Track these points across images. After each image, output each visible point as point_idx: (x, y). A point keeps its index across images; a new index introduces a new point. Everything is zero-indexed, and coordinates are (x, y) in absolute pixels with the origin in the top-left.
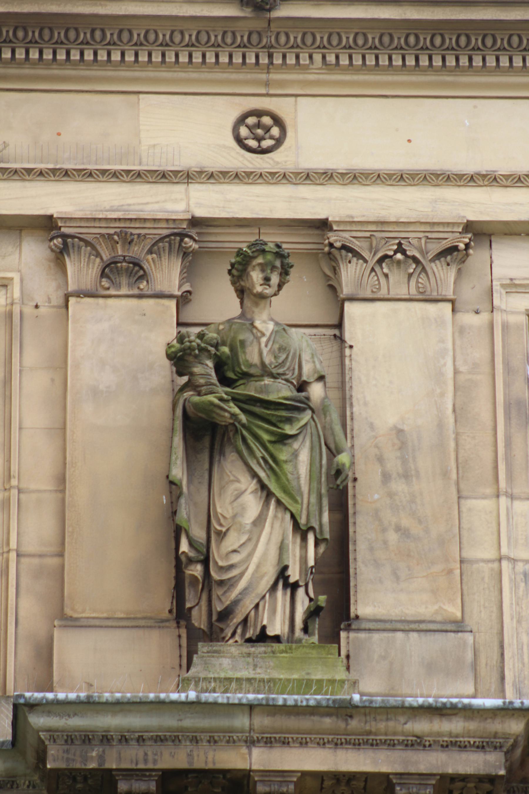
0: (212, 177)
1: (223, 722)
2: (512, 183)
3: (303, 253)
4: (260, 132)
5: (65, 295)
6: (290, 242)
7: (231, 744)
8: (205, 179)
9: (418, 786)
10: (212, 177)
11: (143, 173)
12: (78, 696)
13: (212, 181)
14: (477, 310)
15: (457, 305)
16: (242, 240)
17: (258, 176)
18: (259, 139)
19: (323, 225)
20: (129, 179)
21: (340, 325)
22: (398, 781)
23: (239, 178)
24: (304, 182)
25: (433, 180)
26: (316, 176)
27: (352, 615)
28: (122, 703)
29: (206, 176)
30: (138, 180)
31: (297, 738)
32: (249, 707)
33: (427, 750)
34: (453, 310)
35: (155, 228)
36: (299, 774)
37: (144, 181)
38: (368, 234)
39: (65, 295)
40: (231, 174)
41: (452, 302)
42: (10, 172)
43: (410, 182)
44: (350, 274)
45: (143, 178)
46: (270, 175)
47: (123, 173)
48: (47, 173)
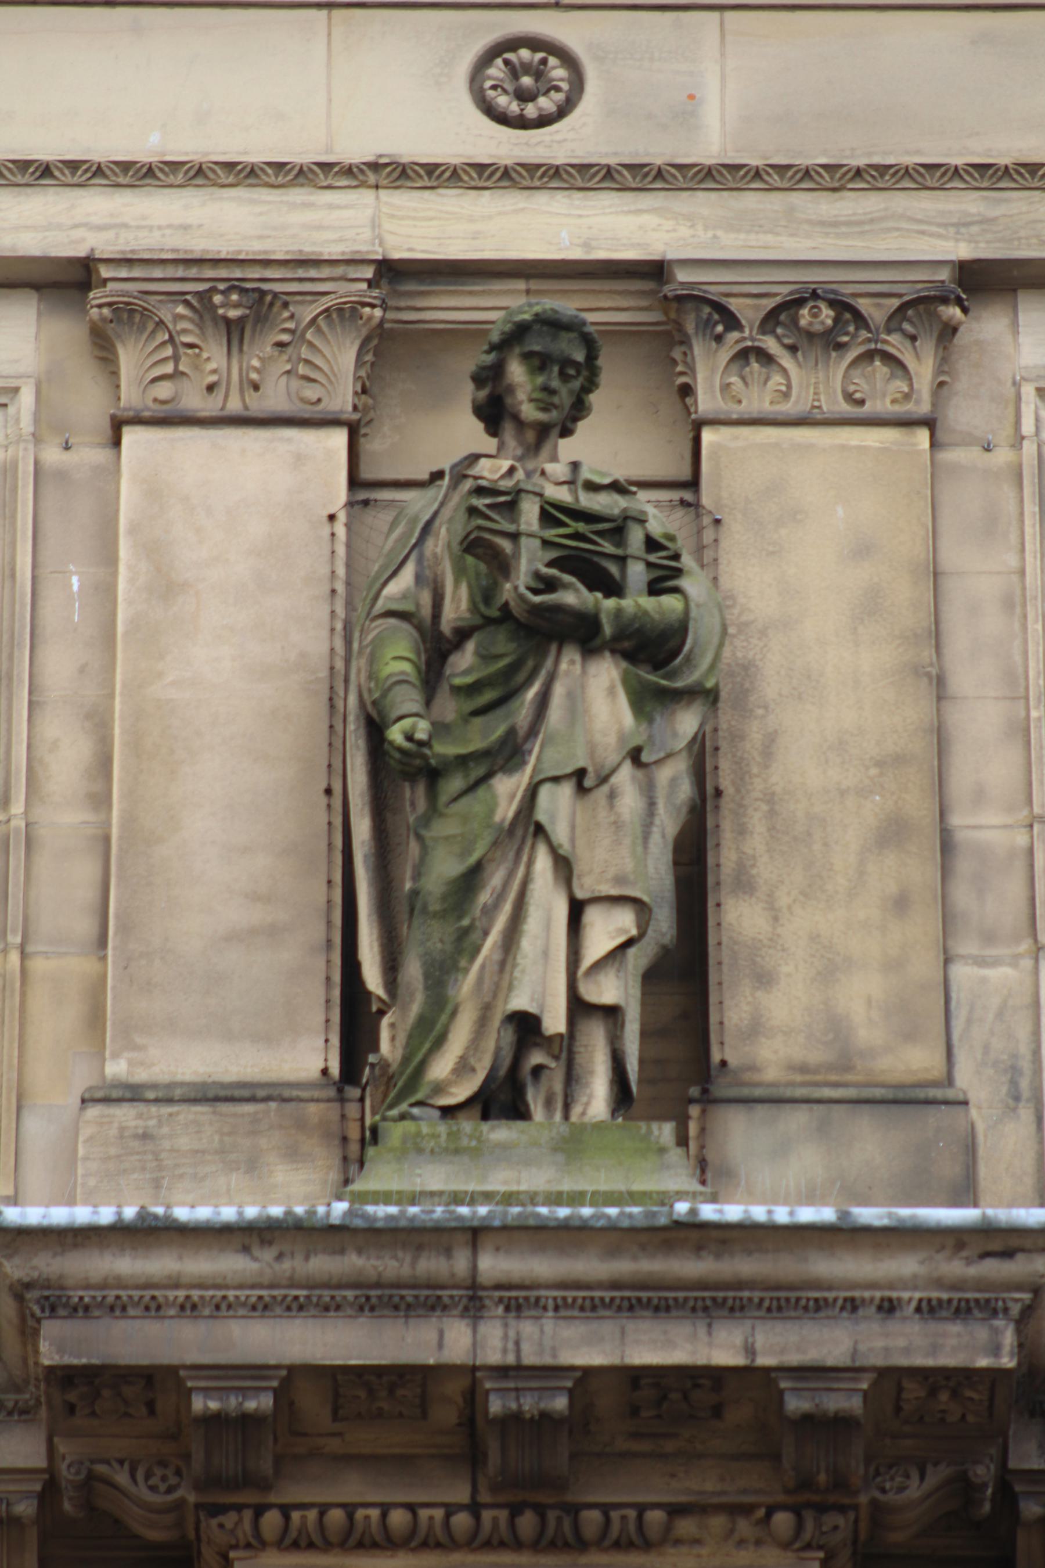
0: (435, 175)
1: (430, 1265)
2: (33, 178)
3: (643, 332)
4: (525, 82)
5: (113, 418)
6: (600, 310)
7: (775, 1314)
8: (33, 178)
9: (536, 1394)
10: (435, 175)
11: (210, 169)
12: (288, 1213)
13: (199, 181)
14: (989, 445)
15: (940, 435)
16: (496, 307)
17: (949, 174)
18: (524, 96)
19: (656, 271)
20: (231, 179)
21: (693, 483)
22: (497, 1385)
23: (511, 179)
24: (850, 186)
25: (523, 177)
26: (1023, 171)
27: (716, 1057)
28: (592, 1229)
29: (37, 169)
30: (658, 185)
31: (575, 1299)
32: (469, 1236)
33: (225, 1317)
34: (934, 444)
35: (301, 280)
36: (872, 1376)
37: (566, 186)
38: (201, 287)
39: (113, 418)
40: (443, 168)
41: (929, 423)
42: (86, 171)
43: (1024, 182)
44: (710, 374)
45: (159, 179)
46: (527, 171)
47: (166, 169)
48: (161, 170)
